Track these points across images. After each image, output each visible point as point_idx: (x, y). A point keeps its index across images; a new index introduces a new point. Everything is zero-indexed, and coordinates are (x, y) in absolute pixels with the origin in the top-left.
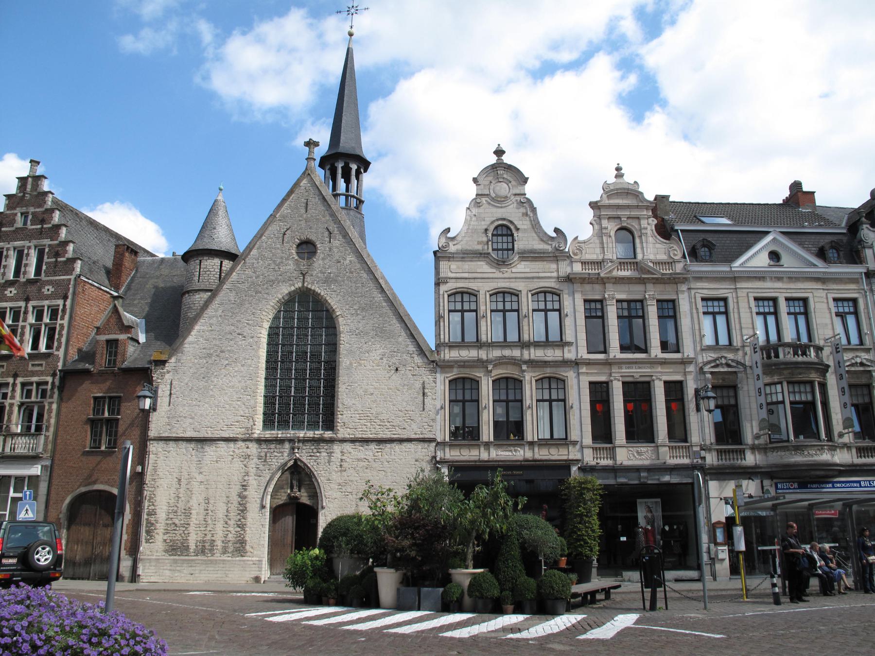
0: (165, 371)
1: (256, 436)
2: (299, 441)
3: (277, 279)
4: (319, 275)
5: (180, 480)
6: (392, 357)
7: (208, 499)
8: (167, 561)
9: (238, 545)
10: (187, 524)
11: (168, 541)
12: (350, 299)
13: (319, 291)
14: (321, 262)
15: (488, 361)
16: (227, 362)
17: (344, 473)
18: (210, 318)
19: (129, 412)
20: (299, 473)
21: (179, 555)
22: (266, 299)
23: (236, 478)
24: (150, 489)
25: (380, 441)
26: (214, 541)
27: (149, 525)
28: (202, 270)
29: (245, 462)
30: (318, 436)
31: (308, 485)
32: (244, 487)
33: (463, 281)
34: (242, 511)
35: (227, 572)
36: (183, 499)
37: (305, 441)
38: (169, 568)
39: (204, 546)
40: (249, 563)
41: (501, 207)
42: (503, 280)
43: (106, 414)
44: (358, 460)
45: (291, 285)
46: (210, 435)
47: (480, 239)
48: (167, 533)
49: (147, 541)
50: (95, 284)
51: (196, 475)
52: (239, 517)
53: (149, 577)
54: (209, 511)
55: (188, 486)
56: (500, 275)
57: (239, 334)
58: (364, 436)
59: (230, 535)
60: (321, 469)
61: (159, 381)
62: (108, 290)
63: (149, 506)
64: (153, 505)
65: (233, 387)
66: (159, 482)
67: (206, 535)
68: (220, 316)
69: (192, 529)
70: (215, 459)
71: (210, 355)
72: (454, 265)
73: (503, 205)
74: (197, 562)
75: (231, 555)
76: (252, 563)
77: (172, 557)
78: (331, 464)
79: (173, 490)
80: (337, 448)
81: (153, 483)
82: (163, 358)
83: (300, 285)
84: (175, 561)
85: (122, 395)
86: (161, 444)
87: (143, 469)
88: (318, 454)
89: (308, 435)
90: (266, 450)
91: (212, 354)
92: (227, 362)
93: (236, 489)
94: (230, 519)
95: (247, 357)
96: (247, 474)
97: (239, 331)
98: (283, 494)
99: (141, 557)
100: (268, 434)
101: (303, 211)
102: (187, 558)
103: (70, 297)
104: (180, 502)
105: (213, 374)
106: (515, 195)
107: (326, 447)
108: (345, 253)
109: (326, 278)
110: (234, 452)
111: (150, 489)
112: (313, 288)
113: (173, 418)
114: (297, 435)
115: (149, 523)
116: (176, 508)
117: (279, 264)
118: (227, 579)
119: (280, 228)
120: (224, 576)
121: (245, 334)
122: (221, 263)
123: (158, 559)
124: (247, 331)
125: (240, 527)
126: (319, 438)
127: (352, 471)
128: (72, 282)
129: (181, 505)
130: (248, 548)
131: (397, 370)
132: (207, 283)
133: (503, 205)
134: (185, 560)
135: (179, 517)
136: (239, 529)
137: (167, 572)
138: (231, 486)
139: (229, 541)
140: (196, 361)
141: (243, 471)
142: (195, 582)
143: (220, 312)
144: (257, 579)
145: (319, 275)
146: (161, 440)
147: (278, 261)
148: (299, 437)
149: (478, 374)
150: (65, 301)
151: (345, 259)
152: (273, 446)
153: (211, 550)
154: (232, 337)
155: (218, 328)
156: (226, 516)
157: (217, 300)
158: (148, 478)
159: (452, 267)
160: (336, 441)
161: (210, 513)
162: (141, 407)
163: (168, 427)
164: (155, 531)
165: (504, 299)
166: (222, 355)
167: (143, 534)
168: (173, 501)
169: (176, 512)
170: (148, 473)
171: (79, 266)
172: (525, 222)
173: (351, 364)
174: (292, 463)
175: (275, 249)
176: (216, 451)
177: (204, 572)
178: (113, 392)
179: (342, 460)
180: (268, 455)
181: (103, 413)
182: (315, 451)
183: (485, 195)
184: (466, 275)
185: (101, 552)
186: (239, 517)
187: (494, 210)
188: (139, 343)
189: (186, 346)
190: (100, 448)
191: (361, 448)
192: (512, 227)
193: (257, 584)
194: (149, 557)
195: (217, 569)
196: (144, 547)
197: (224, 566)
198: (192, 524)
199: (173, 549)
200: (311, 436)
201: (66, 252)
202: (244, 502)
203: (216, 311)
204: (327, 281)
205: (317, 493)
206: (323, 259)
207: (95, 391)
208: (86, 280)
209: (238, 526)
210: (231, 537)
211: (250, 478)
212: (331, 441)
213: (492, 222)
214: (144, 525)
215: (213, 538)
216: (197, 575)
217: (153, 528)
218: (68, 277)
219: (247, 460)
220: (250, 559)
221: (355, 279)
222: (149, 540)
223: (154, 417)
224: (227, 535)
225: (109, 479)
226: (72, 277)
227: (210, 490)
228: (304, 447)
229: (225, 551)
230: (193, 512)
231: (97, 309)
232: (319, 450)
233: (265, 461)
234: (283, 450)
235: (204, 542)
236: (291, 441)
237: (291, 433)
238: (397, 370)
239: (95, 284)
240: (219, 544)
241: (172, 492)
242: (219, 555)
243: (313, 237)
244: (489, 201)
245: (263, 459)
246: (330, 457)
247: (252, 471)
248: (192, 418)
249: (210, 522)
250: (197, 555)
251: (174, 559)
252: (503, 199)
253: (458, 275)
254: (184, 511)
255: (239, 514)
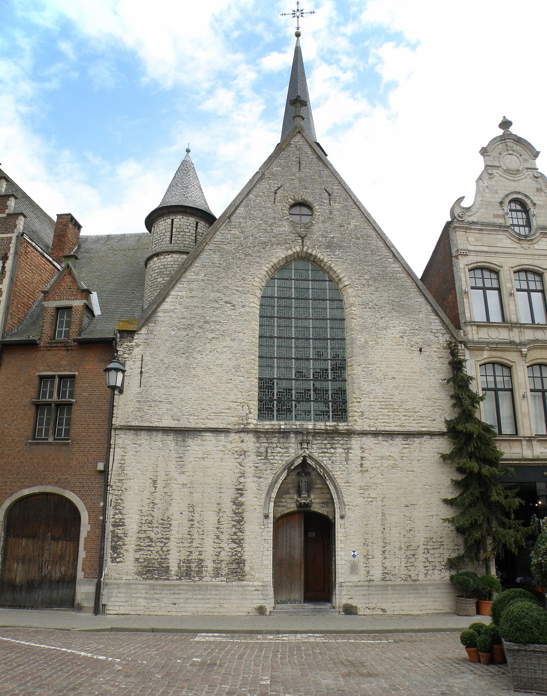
0: (133, 344)
1: (251, 426)
2: (308, 433)
3: (270, 241)
4: (320, 239)
5: (155, 482)
6: (414, 335)
7: (193, 506)
8: (141, 587)
9: (234, 566)
10: (166, 539)
11: (141, 560)
12: (358, 267)
13: (322, 257)
14: (321, 225)
15: (522, 344)
16: (213, 335)
17: (366, 475)
18: (190, 282)
19: (87, 394)
20: (308, 474)
21: (157, 579)
22: (258, 262)
23: (230, 479)
24: (116, 492)
25: (408, 435)
26: (202, 560)
27: (116, 539)
28: (174, 230)
29: (239, 460)
30: (331, 428)
31: (321, 488)
32: (240, 491)
33: (483, 254)
34: (239, 522)
35: (221, 601)
36: (159, 505)
37: (316, 433)
38: (144, 595)
39: (190, 567)
40: (250, 588)
41: (514, 181)
42: (525, 257)
43: (55, 398)
44: (382, 458)
45: (287, 249)
46: (193, 425)
47: (496, 213)
48: (141, 550)
49: (114, 560)
50: (39, 249)
51: (176, 475)
52: (234, 530)
53: (117, 608)
54: (195, 522)
55: (167, 490)
56: (523, 251)
57: (227, 302)
58: (387, 429)
59: (223, 554)
60: (338, 469)
61: (126, 356)
62: (51, 259)
63: (116, 514)
64: (121, 513)
65: (221, 365)
66: (127, 484)
67: (191, 552)
68: (203, 280)
69: (173, 545)
70: (201, 456)
71: (190, 327)
72: (472, 237)
73: (516, 179)
74: (181, 588)
75: (225, 579)
76: (254, 589)
77: (147, 582)
78: (349, 462)
79: (146, 494)
80: (355, 443)
81: (120, 484)
82: (131, 328)
83: (298, 249)
84: (152, 587)
85: (77, 373)
86: (130, 435)
87: (107, 466)
88: (333, 451)
89: (318, 427)
90: (266, 445)
91: (193, 325)
92: (213, 335)
93: (229, 494)
94: (222, 533)
95: (238, 329)
96: (243, 475)
97: (227, 299)
98: (289, 501)
99: (107, 581)
100: (267, 425)
101: (295, 169)
102: (166, 582)
103: (11, 257)
104: (156, 509)
105: (195, 349)
106: (528, 169)
107: (341, 442)
108: (348, 218)
109: (328, 243)
110: (224, 446)
111: (116, 492)
112: (314, 253)
113: (145, 401)
114: (305, 426)
115: (116, 537)
116: (150, 518)
117: (271, 225)
118: (222, 610)
119: (270, 186)
120: (218, 606)
121: (234, 303)
122: (197, 223)
123: (129, 584)
124: (237, 299)
125: (235, 543)
126: (333, 430)
127: (375, 471)
128: (14, 241)
129: (158, 515)
130: (247, 569)
131: (421, 350)
132: (182, 245)
133: (516, 179)
134: (166, 585)
135: (155, 529)
136: (235, 546)
137: (141, 600)
138: (222, 490)
139: (222, 561)
140: (173, 333)
141: (238, 471)
142: (179, 614)
143: (201, 276)
144: (261, 610)
145: (320, 239)
146: (130, 429)
147: (271, 221)
148: (307, 429)
149: (510, 357)
150: (4, 263)
151: (350, 224)
152: (275, 440)
153: (199, 572)
154: (217, 306)
155: (200, 294)
156: (218, 528)
157: (198, 263)
158: (113, 479)
159: (470, 239)
160: (354, 434)
161: (196, 525)
162: (112, 383)
163: (138, 413)
164: (125, 548)
165: (527, 278)
166: (207, 326)
167: (108, 551)
168: (147, 508)
169: (151, 523)
170: (114, 472)
171: (22, 223)
172: (541, 198)
173: (366, 342)
174: (299, 461)
175: (265, 208)
176: (202, 445)
177: (190, 601)
178: (64, 370)
179: (362, 458)
180: (269, 451)
181: (51, 396)
182: (328, 446)
183: (495, 166)
184: (486, 249)
185: (50, 572)
186: (234, 530)
187: (507, 183)
188: (93, 315)
189: (159, 314)
190: (47, 439)
191: (385, 443)
192: (528, 202)
193: (261, 617)
194: (116, 582)
195: (208, 597)
196: (109, 568)
197: (217, 593)
198: (172, 537)
199: (148, 571)
200: (323, 427)
201: (6, 207)
202: (240, 510)
203: (197, 274)
204: (330, 246)
205: (332, 498)
206: (323, 222)
207: (42, 368)
208: (30, 241)
209: (234, 541)
210: (224, 555)
211: (247, 480)
212: (349, 433)
213: (507, 196)
214: (110, 540)
215: (201, 557)
216: (182, 605)
217: (121, 543)
218: (9, 235)
219: (243, 457)
220: (251, 583)
221: (362, 246)
222: (115, 558)
223: (119, 400)
224: (219, 553)
225: (60, 479)
226: (14, 236)
227: (195, 495)
228: (315, 442)
229: (217, 573)
230: (172, 522)
231: (39, 278)
232: (334, 446)
233: (266, 458)
234: (287, 445)
235: (189, 561)
236: (297, 432)
237: (297, 424)
238: (421, 350)
239: (39, 249)
240: (209, 565)
241: (145, 497)
242: (209, 579)
243: (309, 199)
244: (501, 173)
245: (264, 456)
246: (347, 454)
247: (250, 470)
248: (171, 403)
249: (196, 536)
250: (180, 579)
251: (150, 585)
252: (515, 173)
253: (477, 248)
254: (161, 522)
255: (234, 526)
